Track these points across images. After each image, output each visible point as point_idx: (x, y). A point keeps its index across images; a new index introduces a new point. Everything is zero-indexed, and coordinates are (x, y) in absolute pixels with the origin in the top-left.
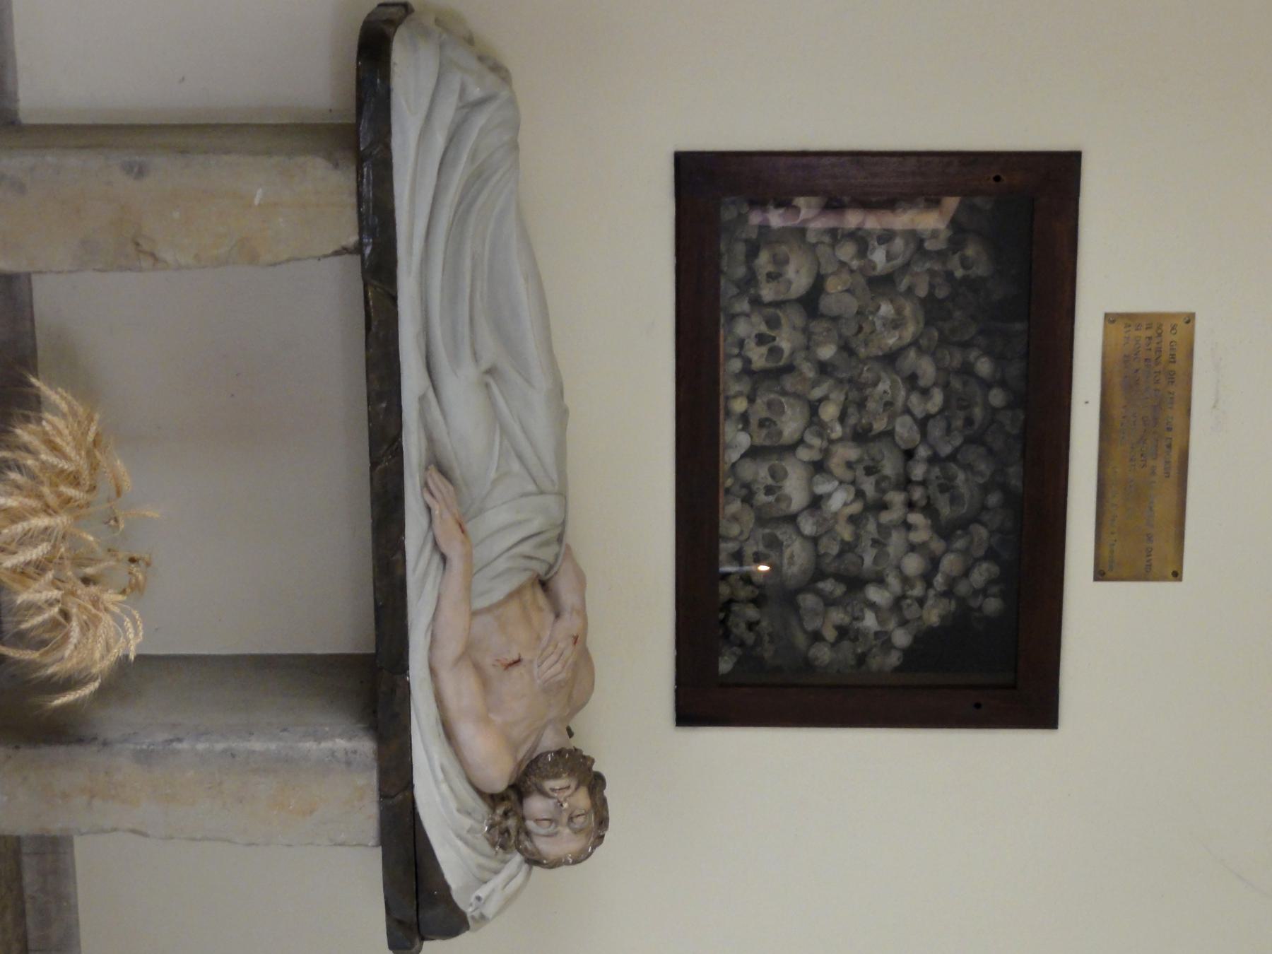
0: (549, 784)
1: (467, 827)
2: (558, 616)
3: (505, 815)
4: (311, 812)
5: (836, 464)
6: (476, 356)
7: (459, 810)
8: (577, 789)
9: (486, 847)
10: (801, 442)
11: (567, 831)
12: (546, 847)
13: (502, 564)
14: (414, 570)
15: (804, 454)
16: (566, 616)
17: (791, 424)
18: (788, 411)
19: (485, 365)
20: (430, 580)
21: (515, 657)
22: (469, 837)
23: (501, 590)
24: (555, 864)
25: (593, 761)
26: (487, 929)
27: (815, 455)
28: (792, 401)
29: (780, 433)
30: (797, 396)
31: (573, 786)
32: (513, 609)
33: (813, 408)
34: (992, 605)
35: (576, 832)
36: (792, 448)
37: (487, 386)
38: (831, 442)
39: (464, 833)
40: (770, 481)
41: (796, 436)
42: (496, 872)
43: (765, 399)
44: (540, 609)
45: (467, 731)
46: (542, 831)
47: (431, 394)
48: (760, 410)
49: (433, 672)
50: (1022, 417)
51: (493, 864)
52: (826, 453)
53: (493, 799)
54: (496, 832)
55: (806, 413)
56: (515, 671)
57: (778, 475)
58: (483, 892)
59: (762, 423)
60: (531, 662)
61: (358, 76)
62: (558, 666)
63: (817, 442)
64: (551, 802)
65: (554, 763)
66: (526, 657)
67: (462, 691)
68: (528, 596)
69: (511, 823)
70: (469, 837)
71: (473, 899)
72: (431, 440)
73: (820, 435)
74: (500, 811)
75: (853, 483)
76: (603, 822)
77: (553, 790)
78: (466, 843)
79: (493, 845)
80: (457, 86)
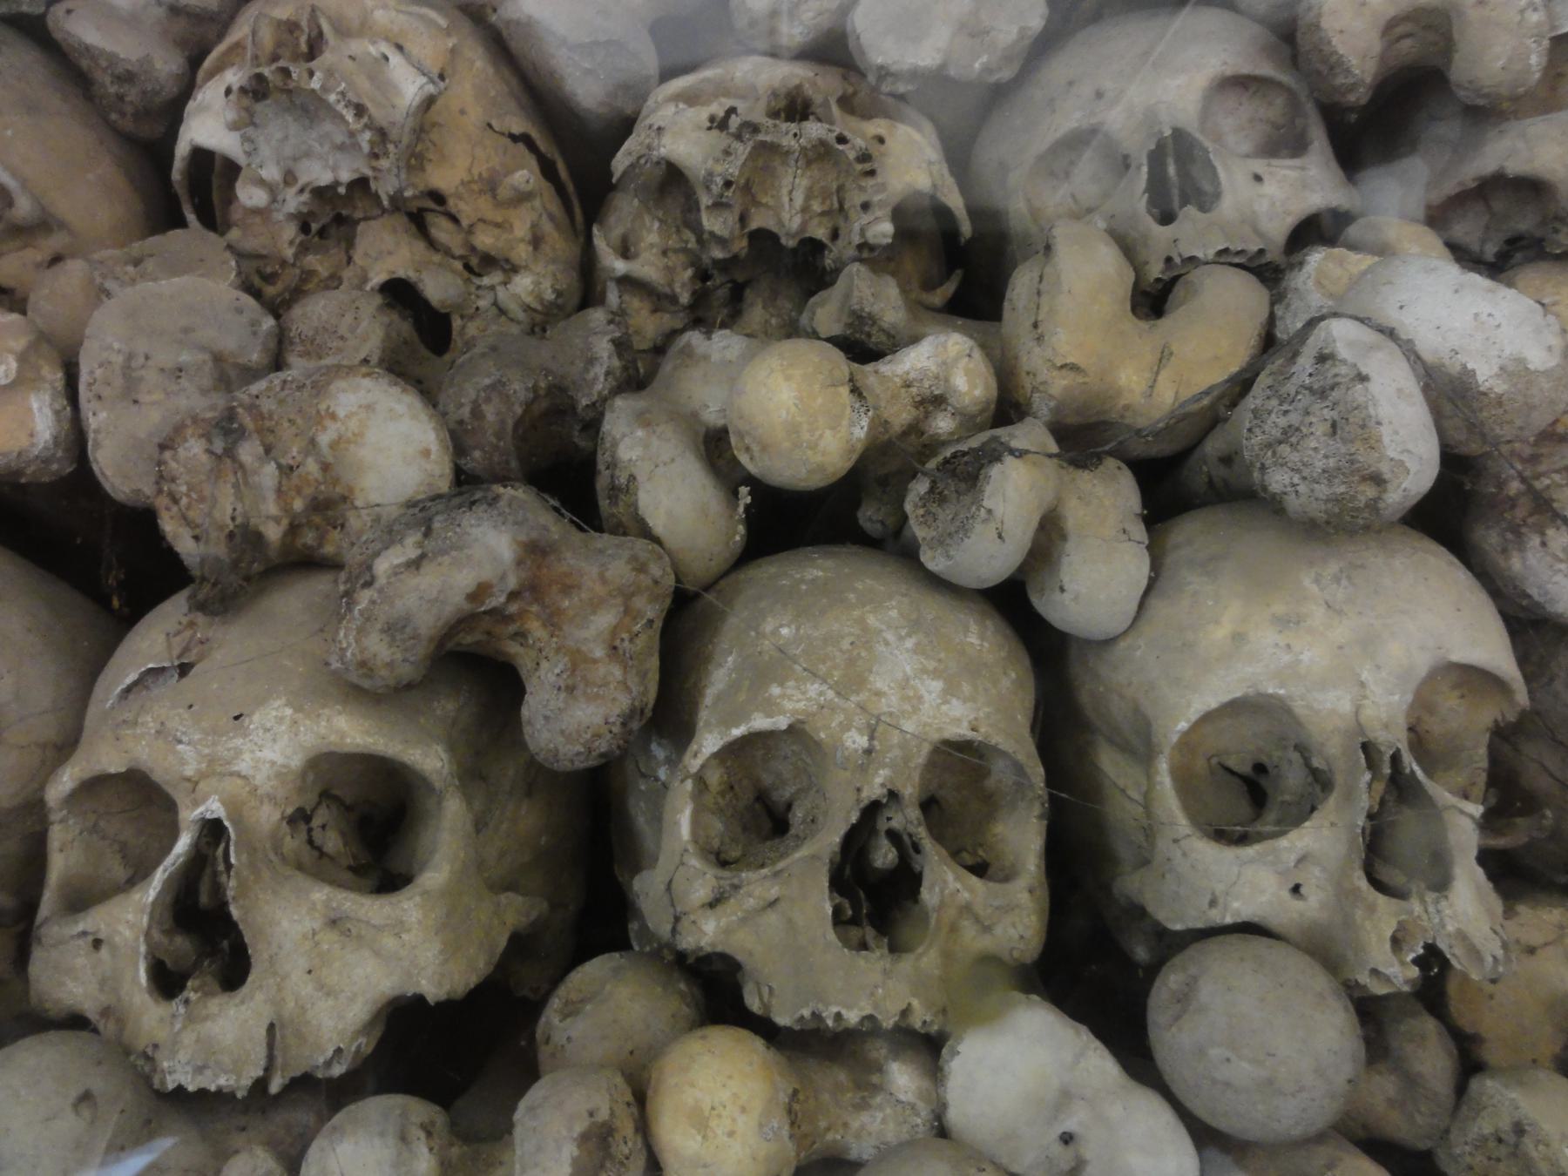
5: (1157, 377)
10: (1011, 602)
15: (1097, 582)
17: (877, 681)
18: (789, 703)
25: (838, 919)
27: (1107, 501)
28: (719, 679)
29: (960, 760)
30: (684, 625)
33: (786, 521)
34: (1353, 117)
36: (1048, 652)
38: (1008, 407)
40: (1323, 840)
41: (980, 637)
43: (700, 883)
47: (626, 1127)
48: (777, 923)
50: (783, 241)
52: (1082, 439)
55: (813, 569)
57: (1252, 789)
59: (874, 896)
61: (660, 830)
63: (1015, 491)
73: (967, 472)
75: (1269, 272)
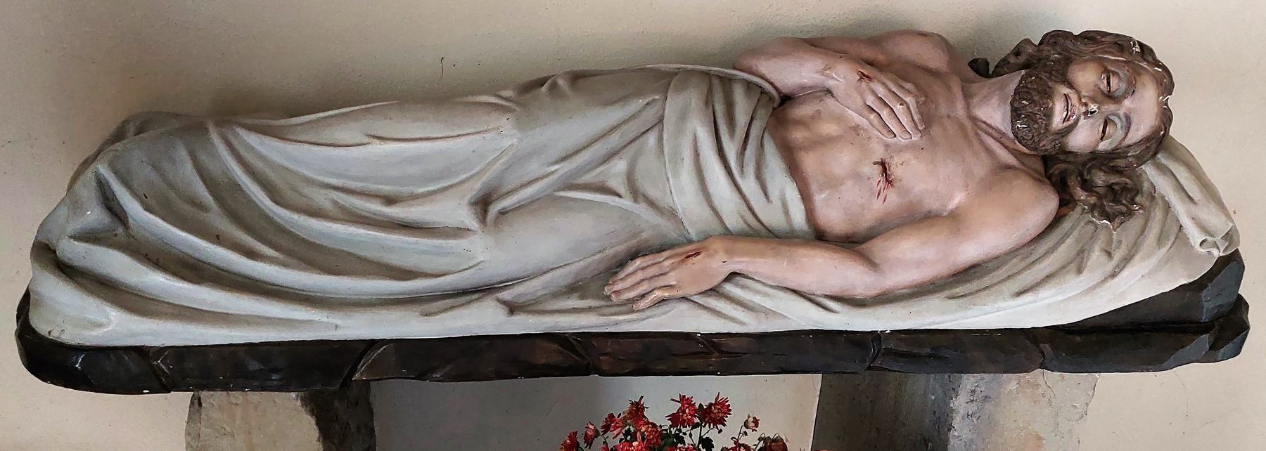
0: (1057, 122)
1: (1104, 258)
2: (829, 92)
3: (1087, 186)
4: (1039, 438)
6: (459, 232)
7: (1079, 271)
8: (1071, 86)
9: (1134, 224)
11: (1127, 103)
12: (1142, 128)
13: (749, 185)
14: (741, 323)
16: (830, 83)
19: (470, 221)
20: (757, 300)
21: (879, 169)
22: (1117, 256)
23: (782, 184)
24: (1166, 117)
25: (1027, 41)
26: (1241, 225)
31: (1066, 90)
32: (809, 162)
35: (1131, 90)
37: (503, 213)
39: (1110, 266)
42: (1167, 207)
44: (817, 116)
45: (970, 251)
46: (1120, 133)
49: (885, 299)
51: (1158, 214)
53: (1066, 203)
54: (1110, 206)
56: (897, 171)
58: (1195, 236)
60: (887, 146)
62: (899, 109)
64: (1082, 121)
65: (1031, 118)
66: (879, 153)
67: (912, 257)
68: (798, 135)
69: (1100, 179)
70: (1117, 256)
71: (1203, 251)
72: (575, 288)
74: (1081, 195)
76: (1121, 44)
77: (1066, 119)
78: (1127, 260)
79: (1129, 214)
80: (81, 247)
